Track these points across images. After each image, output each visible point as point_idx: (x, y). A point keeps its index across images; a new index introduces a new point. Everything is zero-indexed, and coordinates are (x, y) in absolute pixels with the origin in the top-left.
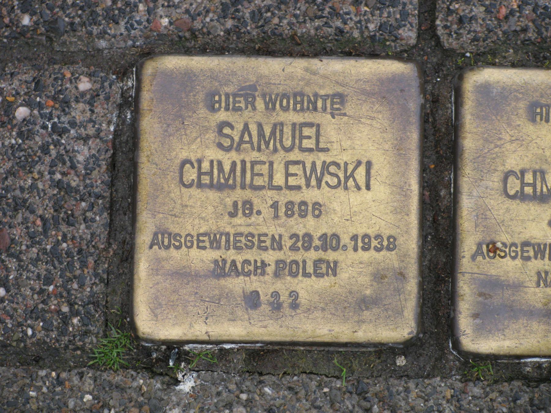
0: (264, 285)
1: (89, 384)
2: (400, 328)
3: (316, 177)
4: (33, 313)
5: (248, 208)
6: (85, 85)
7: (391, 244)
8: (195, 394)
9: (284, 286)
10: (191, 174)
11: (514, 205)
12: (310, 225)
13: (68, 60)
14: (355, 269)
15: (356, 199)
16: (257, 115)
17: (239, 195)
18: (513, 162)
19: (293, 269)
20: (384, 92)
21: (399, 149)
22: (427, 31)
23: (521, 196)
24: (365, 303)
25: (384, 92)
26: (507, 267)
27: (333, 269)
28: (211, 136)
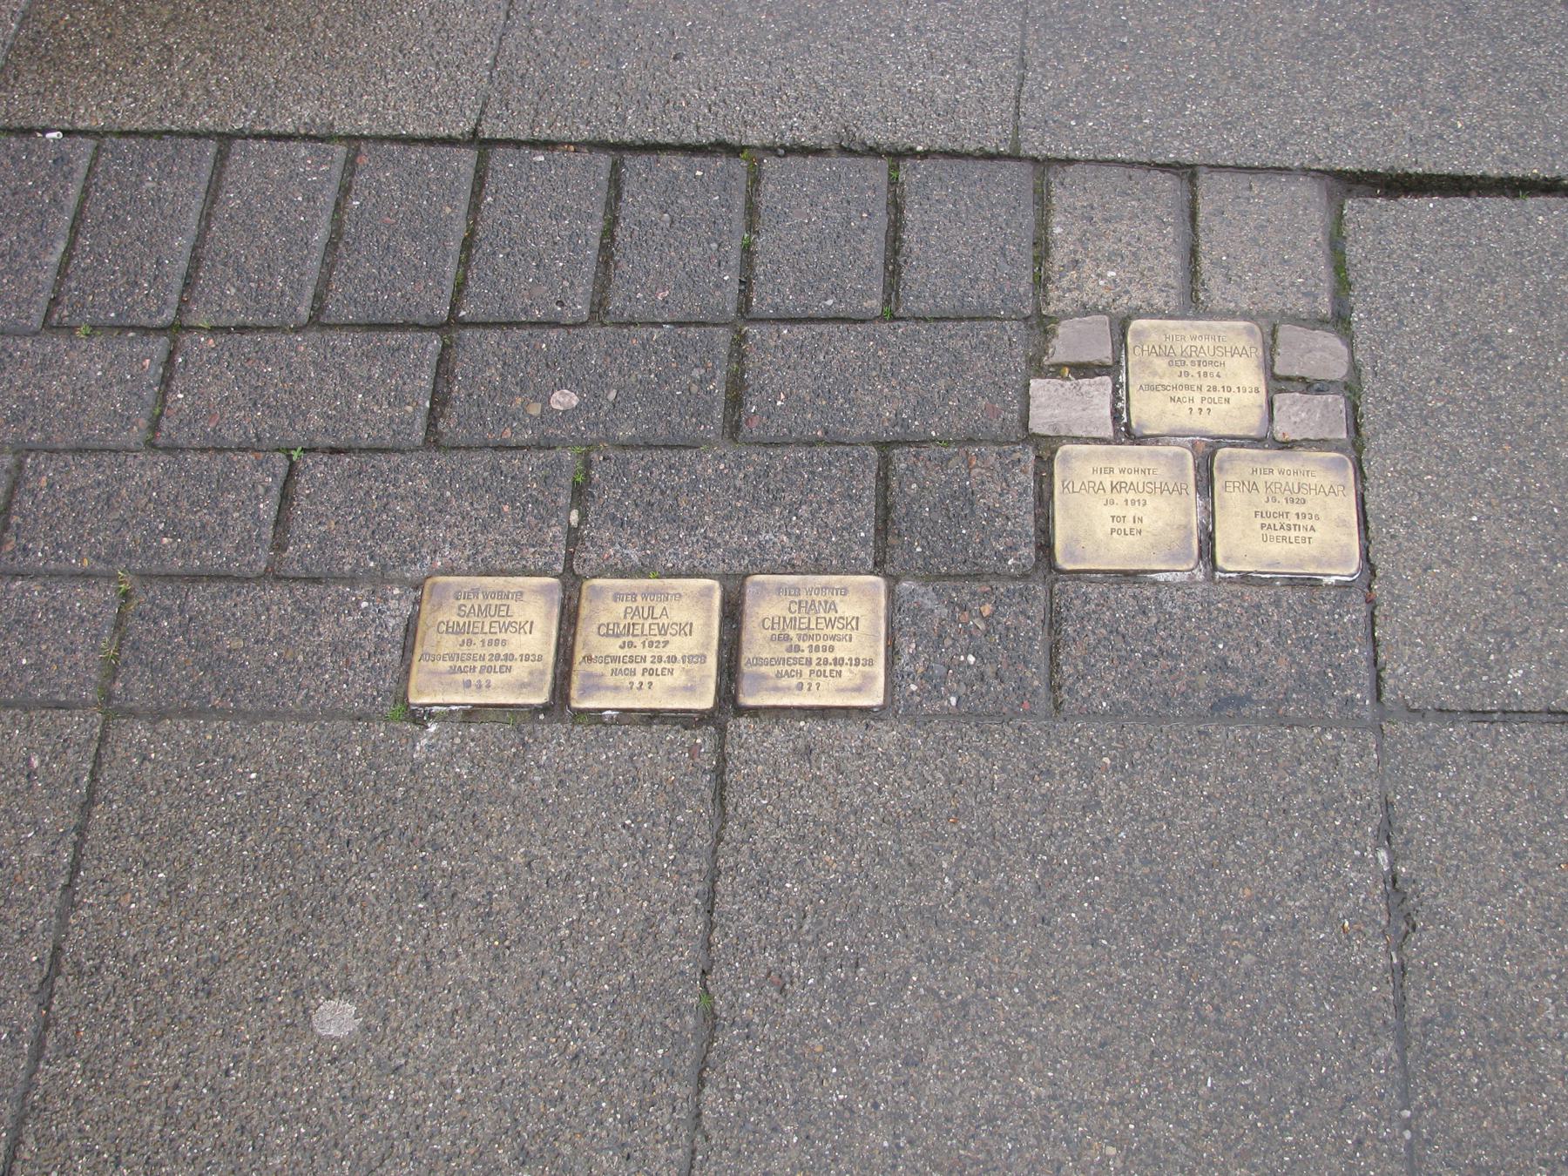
0: (474, 678)
1: (383, 727)
2: (540, 699)
3: (505, 628)
4: (358, 696)
5: (470, 642)
6: (397, 591)
7: (540, 658)
8: (436, 734)
9: (483, 678)
10: (444, 628)
11: (606, 640)
12: (500, 650)
13: (391, 582)
14: (520, 670)
15: (523, 638)
16: (480, 601)
17: (465, 637)
18: (604, 620)
19: (490, 670)
20: (544, 591)
21: (548, 616)
22: (568, 568)
23: (607, 635)
24: (523, 685)
25: (544, 591)
26: (597, 668)
27: (509, 669)
28: (455, 610)
